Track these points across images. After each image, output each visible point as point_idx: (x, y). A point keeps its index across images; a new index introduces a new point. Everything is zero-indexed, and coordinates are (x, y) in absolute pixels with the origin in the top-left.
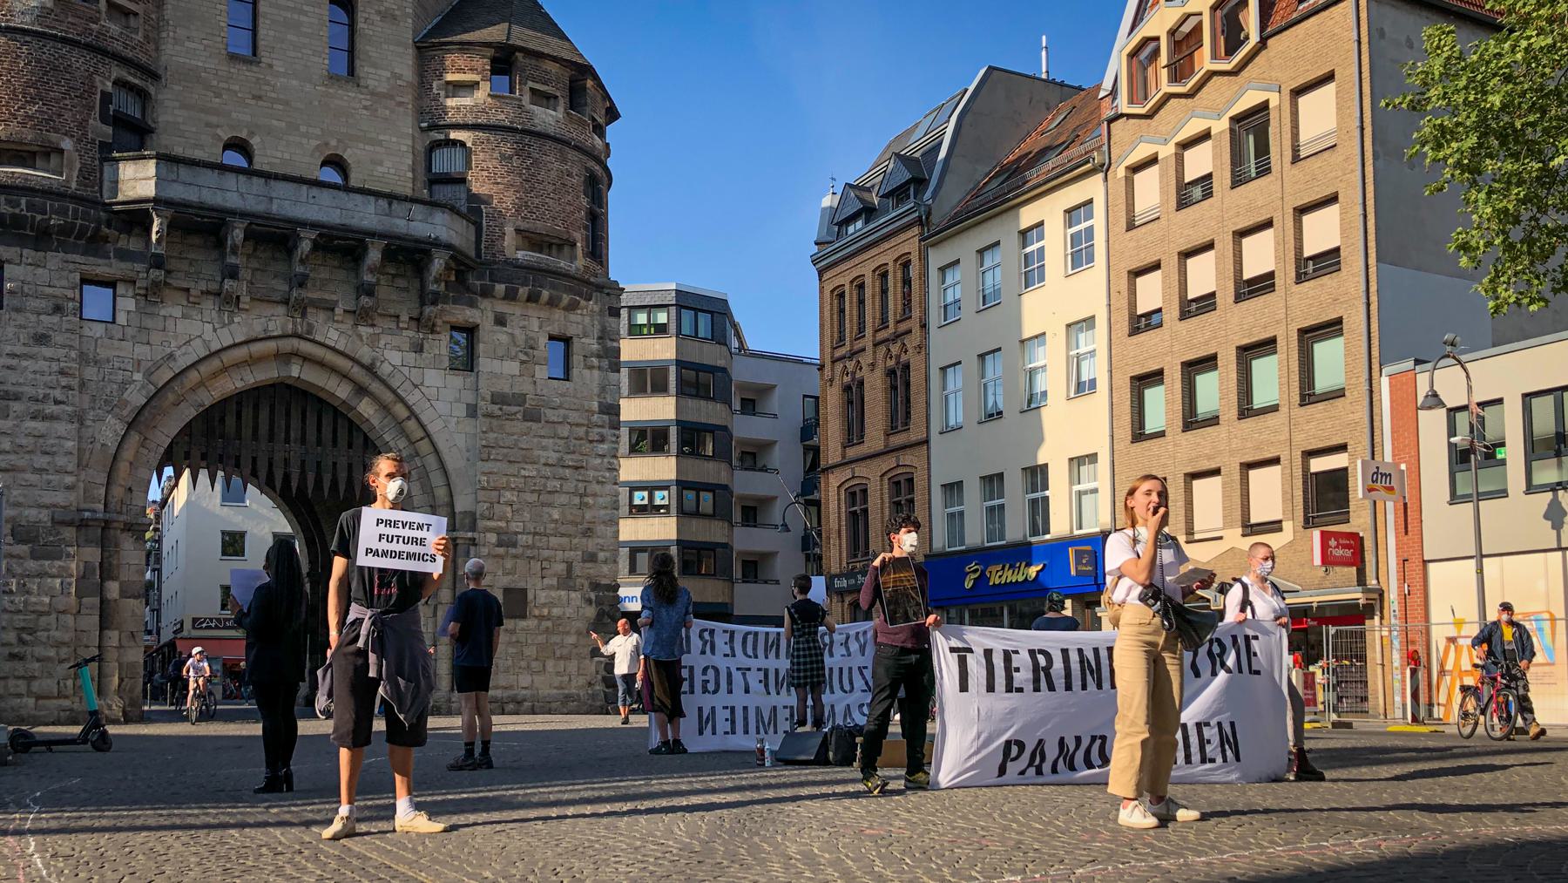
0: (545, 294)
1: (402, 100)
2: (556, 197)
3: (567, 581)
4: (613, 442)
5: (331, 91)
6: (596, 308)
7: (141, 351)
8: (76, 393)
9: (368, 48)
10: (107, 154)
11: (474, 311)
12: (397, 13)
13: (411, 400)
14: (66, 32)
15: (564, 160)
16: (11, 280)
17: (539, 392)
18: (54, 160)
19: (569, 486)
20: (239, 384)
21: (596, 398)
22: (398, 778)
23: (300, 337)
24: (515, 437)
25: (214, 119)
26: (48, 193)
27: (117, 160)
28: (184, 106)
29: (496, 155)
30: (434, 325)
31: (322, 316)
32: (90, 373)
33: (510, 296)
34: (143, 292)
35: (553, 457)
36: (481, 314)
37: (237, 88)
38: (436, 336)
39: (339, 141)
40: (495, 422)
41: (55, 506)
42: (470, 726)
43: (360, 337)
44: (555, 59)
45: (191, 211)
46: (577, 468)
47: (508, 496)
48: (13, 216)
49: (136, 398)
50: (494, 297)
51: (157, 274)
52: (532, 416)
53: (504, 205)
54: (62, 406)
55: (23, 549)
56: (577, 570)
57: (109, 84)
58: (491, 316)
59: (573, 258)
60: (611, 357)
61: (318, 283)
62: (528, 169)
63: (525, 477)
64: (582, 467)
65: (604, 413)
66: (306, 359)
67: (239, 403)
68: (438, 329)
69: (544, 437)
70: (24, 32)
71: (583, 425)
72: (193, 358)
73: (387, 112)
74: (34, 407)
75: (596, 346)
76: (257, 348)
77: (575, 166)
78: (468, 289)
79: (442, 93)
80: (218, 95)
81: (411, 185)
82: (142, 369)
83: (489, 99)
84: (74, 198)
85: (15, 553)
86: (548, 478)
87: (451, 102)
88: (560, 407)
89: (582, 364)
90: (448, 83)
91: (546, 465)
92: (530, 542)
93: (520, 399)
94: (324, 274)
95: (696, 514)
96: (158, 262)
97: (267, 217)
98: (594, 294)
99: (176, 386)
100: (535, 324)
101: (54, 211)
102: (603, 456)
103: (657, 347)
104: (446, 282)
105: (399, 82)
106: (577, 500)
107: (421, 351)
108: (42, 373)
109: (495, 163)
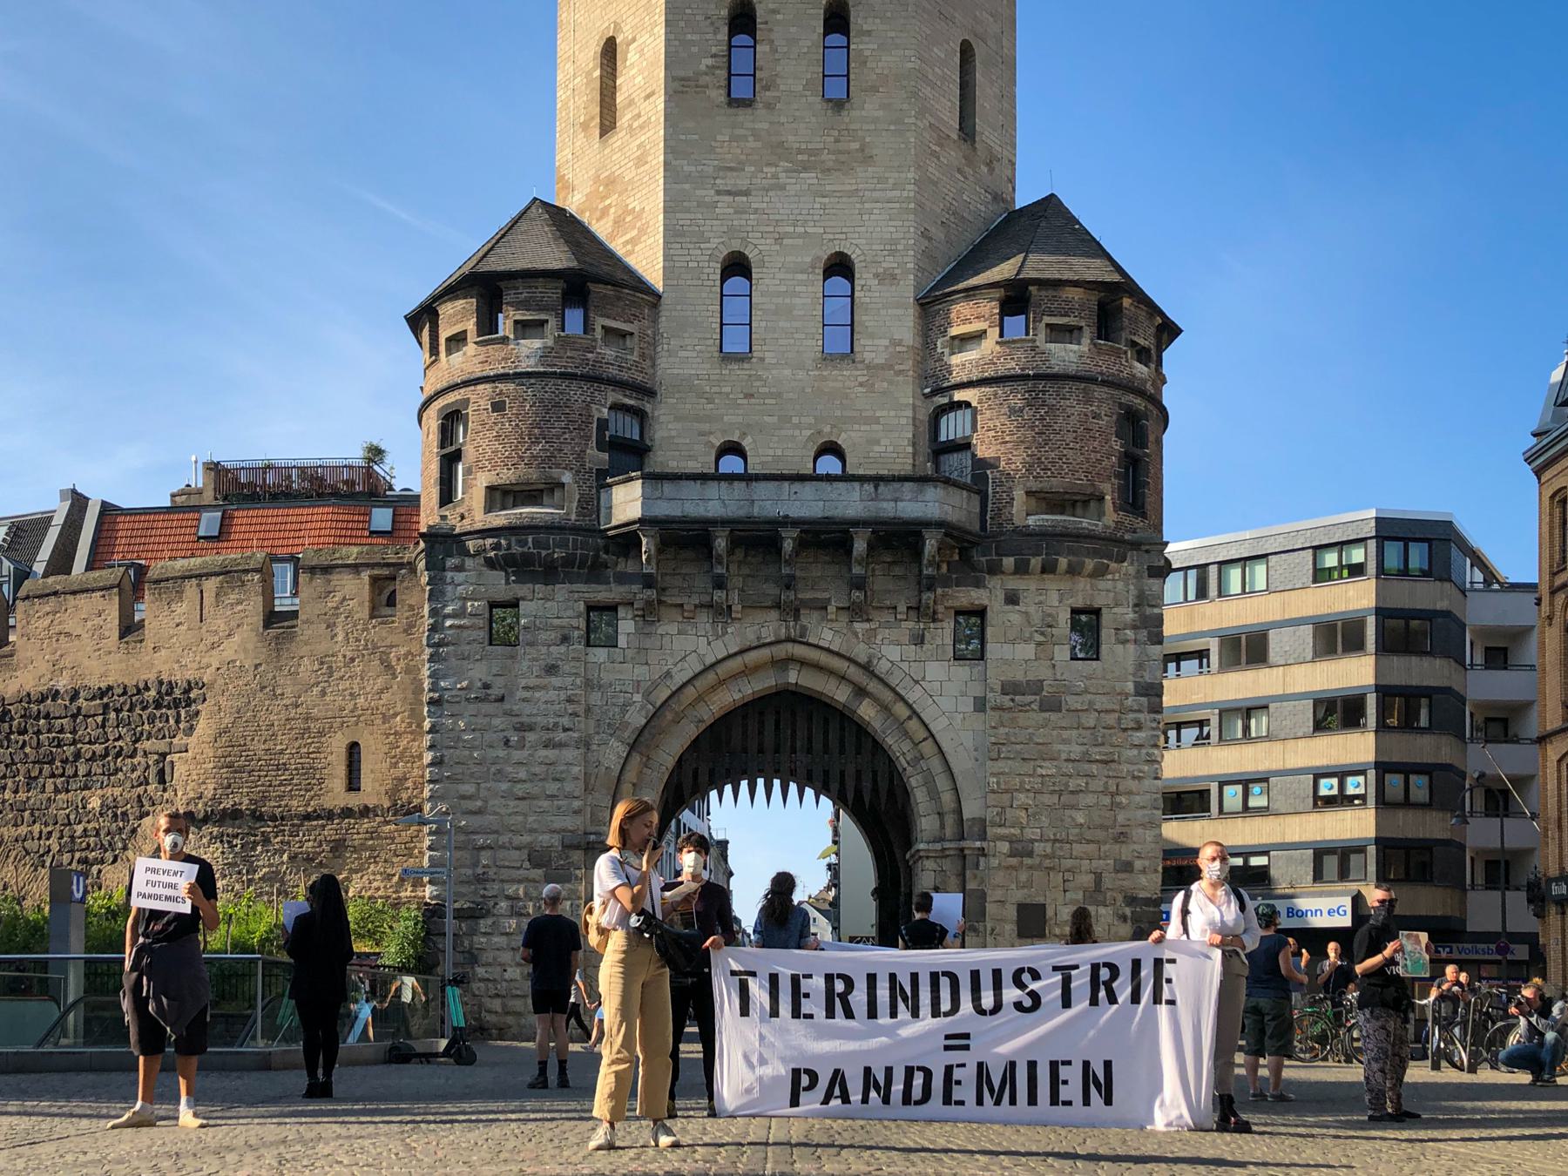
0: (1063, 562)
1: (902, 367)
2: (1078, 446)
4: (1153, 729)
5: (825, 373)
6: (1132, 570)
7: (640, 672)
8: (583, 719)
9: (864, 318)
10: (602, 480)
11: (981, 591)
12: (896, 271)
13: (911, 697)
14: (565, 367)
15: (1088, 401)
16: (525, 616)
17: (1059, 677)
18: (557, 494)
19: (1097, 785)
20: (737, 696)
21: (1131, 677)
22: (181, 1079)
23: (794, 641)
24: (1030, 730)
25: (706, 427)
26: (550, 528)
27: (610, 486)
28: (678, 419)
29: (1005, 410)
30: (935, 612)
31: (816, 615)
32: (596, 698)
33: (1022, 569)
34: (640, 613)
35: (1076, 751)
36: (989, 595)
37: (728, 389)
38: (939, 625)
39: (833, 426)
40: (1006, 716)
41: (564, 830)
42: (542, 1047)
43: (856, 634)
44: (1075, 284)
45: (674, 526)
46: (1106, 762)
47: (1022, 798)
48: (523, 554)
49: (637, 719)
50: (1003, 573)
51: (651, 594)
52: (1051, 705)
53: (1013, 466)
54: (570, 733)
55: (538, 873)
56: (1107, 882)
57: (606, 410)
58: (1001, 596)
59: (1101, 515)
60: (1152, 627)
61: (809, 583)
62: (1042, 419)
63: (1042, 776)
64: (1113, 761)
65: (1142, 695)
66: (803, 663)
67: (745, 717)
68: (940, 616)
69: (1066, 728)
70: (529, 375)
71: (1113, 711)
72: (689, 674)
73: (885, 384)
74: (546, 736)
75: (1131, 616)
76: (752, 657)
77: (1104, 406)
78: (974, 569)
79: (947, 351)
80: (710, 401)
81: (911, 461)
82: (641, 691)
83: (998, 348)
84: (575, 530)
85: (531, 877)
86: (1070, 776)
87: (956, 360)
88: (1086, 691)
89: (1113, 639)
90: (953, 338)
91: (1067, 760)
92: (1049, 850)
93: (1036, 687)
94: (816, 571)
95: (1407, 803)
96: (648, 581)
97: (749, 521)
98: (1129, 554)
99: (673, 704)
100: (1054, 598)
101: (556, 546)
102: (1141, 746)
103: (1351, 593)
104: (949, 563)
105: (898, 349)
106: (1107, 800)
107: (922, 642)
108: (552, 703)
109: (1003, 419)
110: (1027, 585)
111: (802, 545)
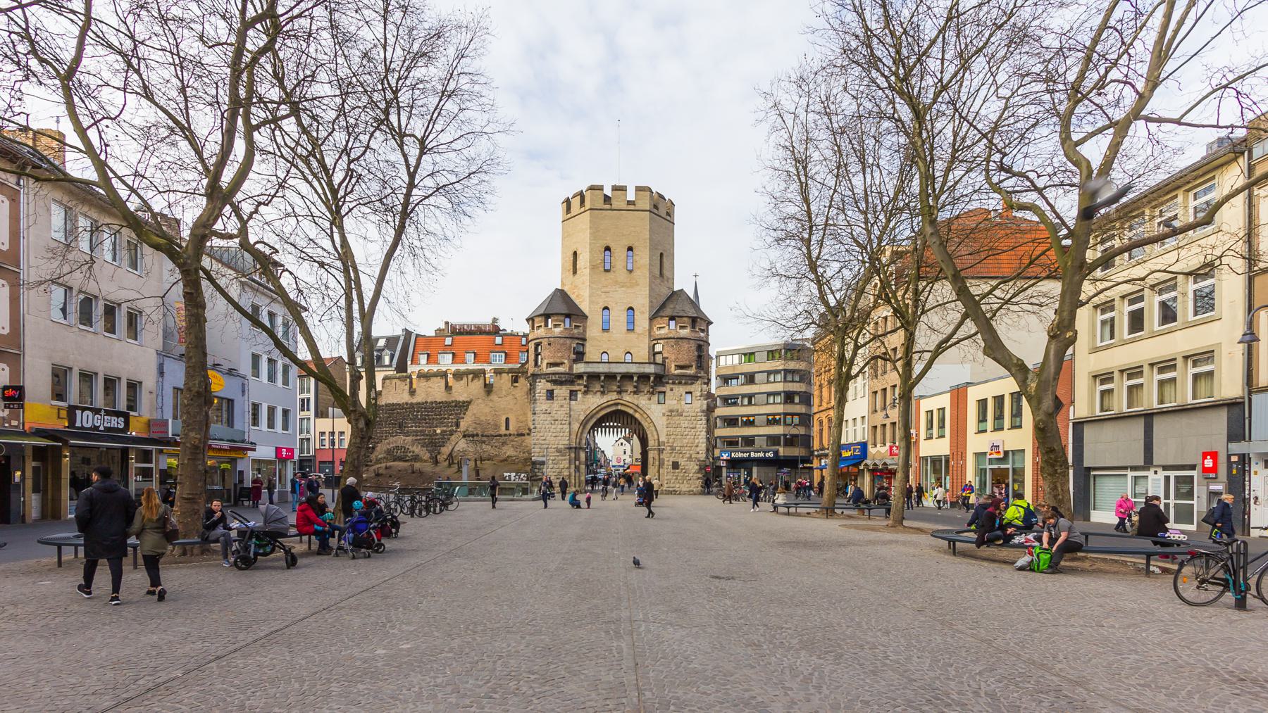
3: (690, 458)
7: (583, 407)
33: (674, 383)
77: (693, 346)
110: (676, 388)
111: (621, 378)
